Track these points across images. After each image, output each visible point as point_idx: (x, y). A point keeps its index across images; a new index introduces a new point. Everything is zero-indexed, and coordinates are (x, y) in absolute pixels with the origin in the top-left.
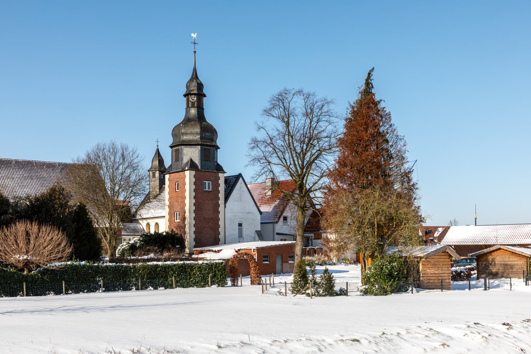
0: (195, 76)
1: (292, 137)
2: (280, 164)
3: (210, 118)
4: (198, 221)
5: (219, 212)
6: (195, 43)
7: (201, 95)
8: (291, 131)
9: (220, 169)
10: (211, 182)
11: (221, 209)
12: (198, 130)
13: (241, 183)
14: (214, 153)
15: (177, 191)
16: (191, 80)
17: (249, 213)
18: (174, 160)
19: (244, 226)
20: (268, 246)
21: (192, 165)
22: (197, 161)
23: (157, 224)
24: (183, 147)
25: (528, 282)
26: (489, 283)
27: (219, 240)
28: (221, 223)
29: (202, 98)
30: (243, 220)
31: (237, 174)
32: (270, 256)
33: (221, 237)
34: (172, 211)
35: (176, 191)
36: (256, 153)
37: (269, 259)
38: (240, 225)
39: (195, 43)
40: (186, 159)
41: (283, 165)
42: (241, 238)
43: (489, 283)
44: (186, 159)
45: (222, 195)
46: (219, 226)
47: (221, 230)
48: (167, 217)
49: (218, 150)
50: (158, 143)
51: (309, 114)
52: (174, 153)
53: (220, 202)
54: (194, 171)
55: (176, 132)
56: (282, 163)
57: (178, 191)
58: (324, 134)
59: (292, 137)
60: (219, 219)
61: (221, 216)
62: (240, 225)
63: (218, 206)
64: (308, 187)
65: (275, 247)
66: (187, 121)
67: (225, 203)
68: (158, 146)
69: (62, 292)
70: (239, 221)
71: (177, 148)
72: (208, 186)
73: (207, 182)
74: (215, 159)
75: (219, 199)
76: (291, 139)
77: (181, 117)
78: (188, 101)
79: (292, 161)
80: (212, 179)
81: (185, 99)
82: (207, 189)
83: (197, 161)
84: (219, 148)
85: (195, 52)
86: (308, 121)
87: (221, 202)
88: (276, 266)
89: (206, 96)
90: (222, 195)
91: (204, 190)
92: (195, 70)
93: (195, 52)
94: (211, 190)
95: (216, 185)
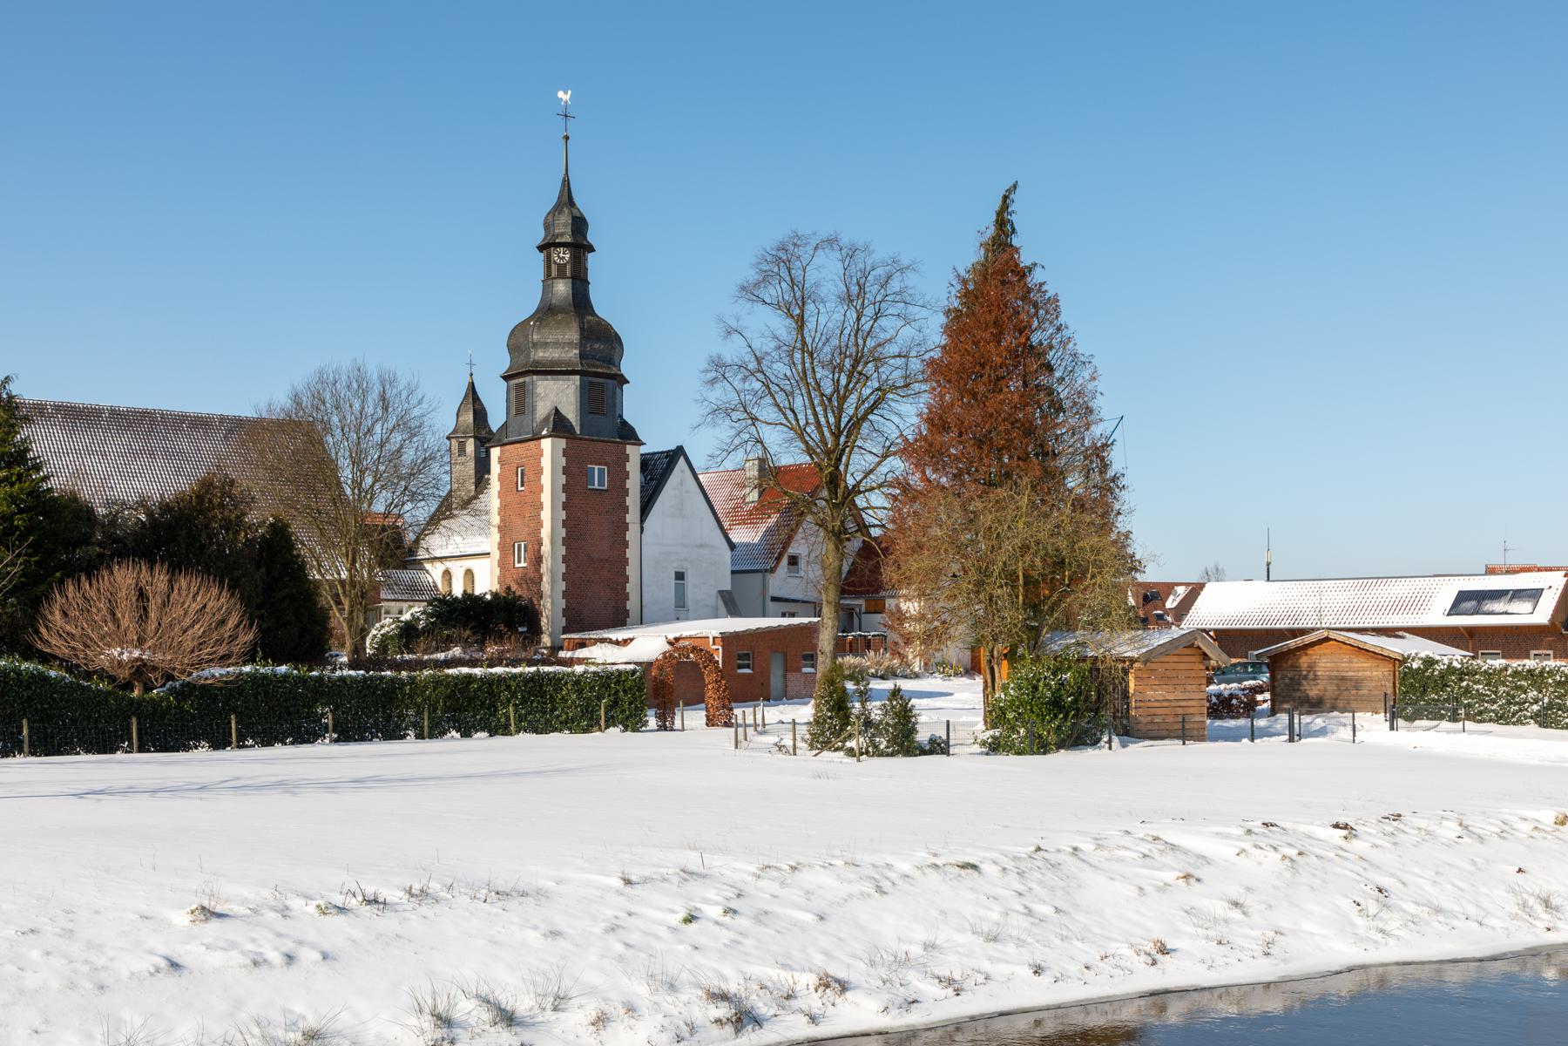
0: (566, 199)
1: (811, 355)
2: (781, 424)
3: (604, 303)
4: (573, 566)
5: (626, 544)
6: (566, 116)
7: (581, 248)
8: (809, 340)
9: (628, 434)
10: (606, 468)
11: (632, 535)
12: (573, 335)
13: (682, 471)
14: (614, 393)
15: (520, 488)
16: (558, 209)
17: (702, 546)
18: (513, 411)
19: (690, 580)
20: (751, 630)
21: (559, 425)
22: (571, 414)
23: (469, 573)
24: (535, 377)
25: (1395, 722)
26: (1300, 723)
27: (626, 614)
28: (632, 571)
29: (584, 255)
30: (686, 565)
31: (673, 447)
32: (756, 655)
33: (633, 605)
34: (508, 540)
35: (518, 491)
36: (721, 394)
37: (753, 662)
38: (680, 576)
39: (566, 116)
40: (542, 410)
41: (788, 427)
42: (681, 609)
43: (1300, 723)
44: (542, 410)
45: (633, 501)
46: (627, 579)
47: (632, 588)
48: (496, 554)
49: (625, 386)
50: (474, 367)
51: (853, 297)
52: (513, 393)
53: (629, 518)
54: (564, 440)
55: (518, 340)
56: (785, 422)
57: (523, 488)
58: (893, 349)
59: (811, 355)
60: (626, 561)
61: (631, 553)
62: (680, 576)
63: (626, 527)
64: (851, 482)
65: (768, 632)
66: (547, 312)
67: (642, 521)
68: (471, 375)
69: (230, 744)
70: (675, 565)
71: (521, 380)
72: (599, 476)
73: (596, 467)
74: (618, 410)
75: (626, 510)
76: (807, 360)
77: (530, 303)
78: (548, 260)
79: (812, 417)
80: (609, 459)
81: (541, 256)
82: (596, 486)
83: (571, 414)
84: (627, 382)
85: (567, 138)
86: (852, 315)
87: (633, 517)
88: (769, 679)
89: (593, 250)
90: (633, 501)
91: (589, 487)
92: (566, 183)
93: (567, 138)
94: (606, 487)
95: (620, 476)
